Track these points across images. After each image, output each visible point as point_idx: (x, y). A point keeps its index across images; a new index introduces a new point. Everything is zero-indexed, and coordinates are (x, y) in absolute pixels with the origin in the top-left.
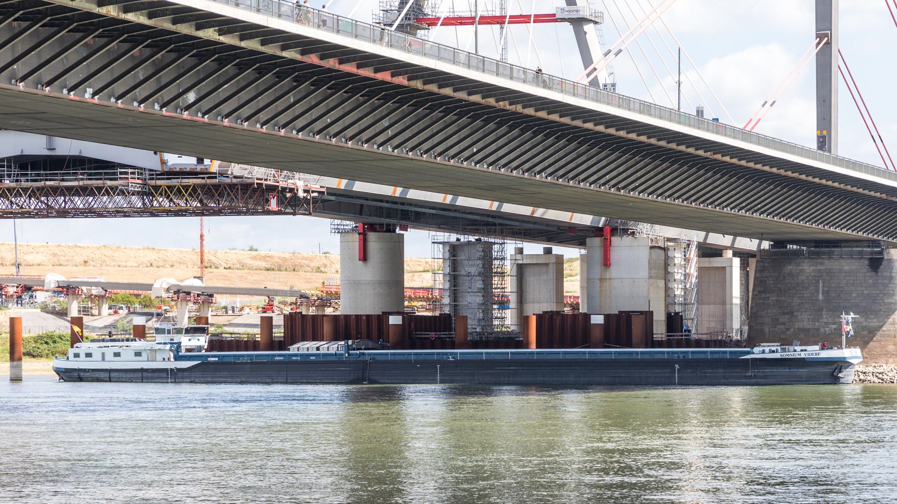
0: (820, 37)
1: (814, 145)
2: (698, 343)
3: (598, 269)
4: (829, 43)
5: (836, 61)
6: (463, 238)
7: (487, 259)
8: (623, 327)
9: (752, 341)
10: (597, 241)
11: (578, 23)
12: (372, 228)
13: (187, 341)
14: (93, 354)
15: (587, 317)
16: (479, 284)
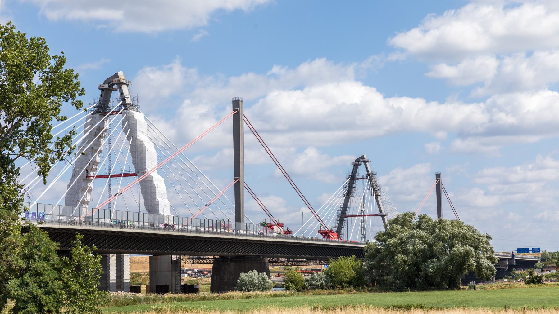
0: (236, 179)
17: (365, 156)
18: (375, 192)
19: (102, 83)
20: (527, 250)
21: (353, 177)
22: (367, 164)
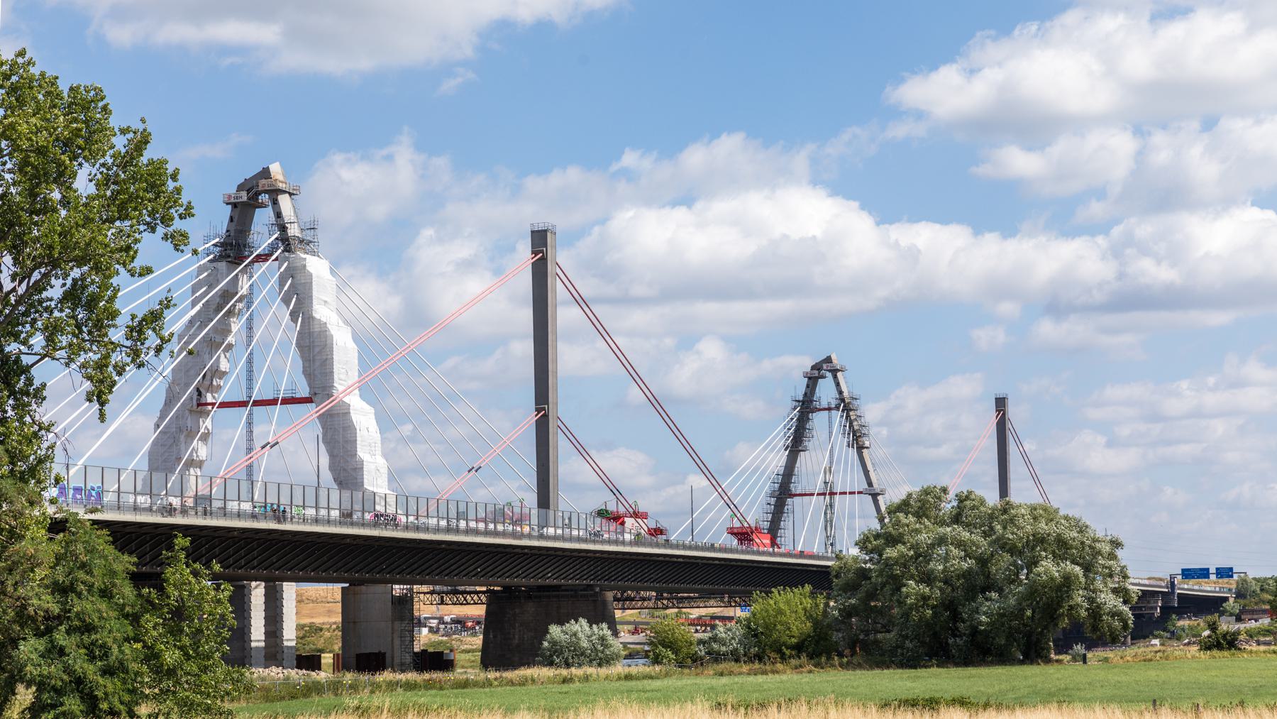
0: (538, 411)
17: (834, 357)
18: (857, 439)
19: (233, 190)
20: (1204, 573)
21: (807, 406)
22: (839, 374)
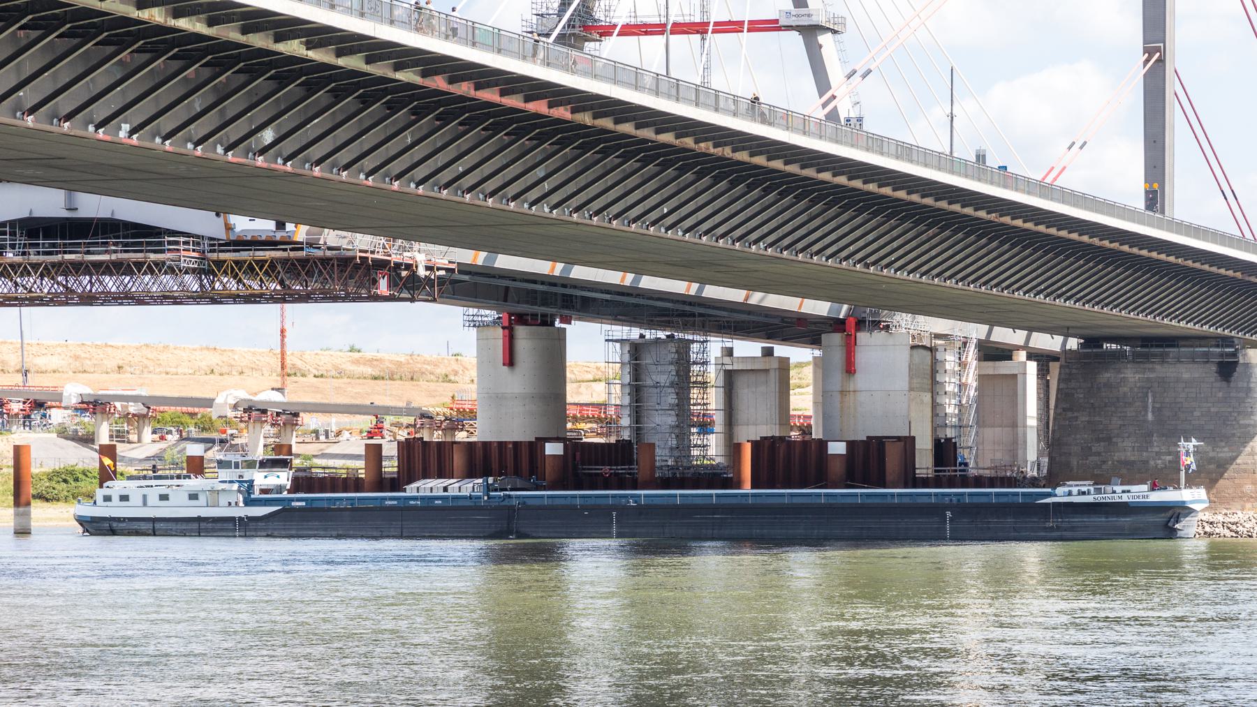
0: (1150, 52)
1: (1140, 204)
2: (979, 482)
3: (837, 377)
4: (1161, 61)
5: (1172, 85)
6: (649, 334)
7: (683, 363)
8: (872, 459)
9: (1054, 478)
10: (836, 339)
11: (810, 32)
12: (522, 319)
13: (261, 479)
14: (131, 497)
15: (822, 444)
16: (672, 399)
